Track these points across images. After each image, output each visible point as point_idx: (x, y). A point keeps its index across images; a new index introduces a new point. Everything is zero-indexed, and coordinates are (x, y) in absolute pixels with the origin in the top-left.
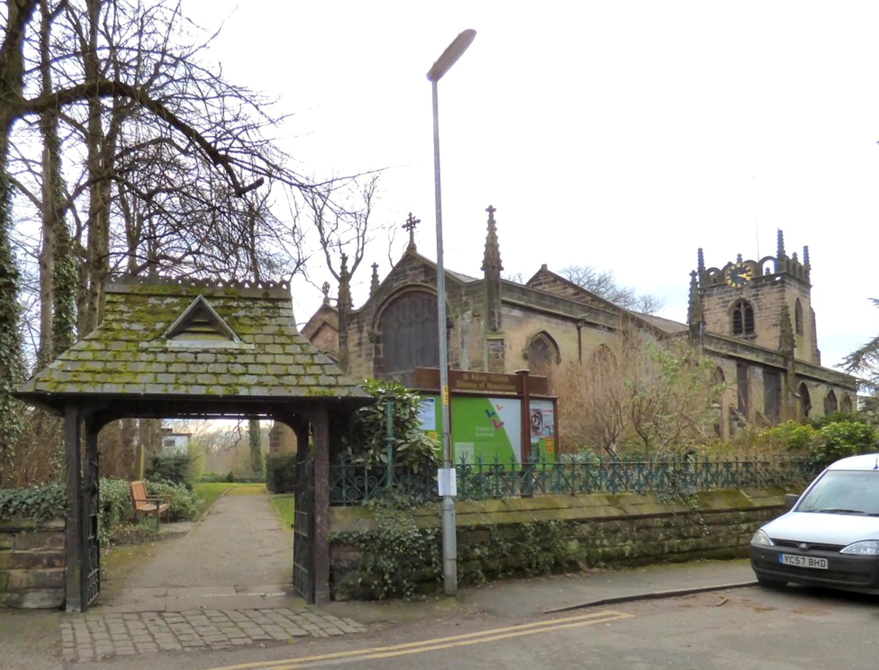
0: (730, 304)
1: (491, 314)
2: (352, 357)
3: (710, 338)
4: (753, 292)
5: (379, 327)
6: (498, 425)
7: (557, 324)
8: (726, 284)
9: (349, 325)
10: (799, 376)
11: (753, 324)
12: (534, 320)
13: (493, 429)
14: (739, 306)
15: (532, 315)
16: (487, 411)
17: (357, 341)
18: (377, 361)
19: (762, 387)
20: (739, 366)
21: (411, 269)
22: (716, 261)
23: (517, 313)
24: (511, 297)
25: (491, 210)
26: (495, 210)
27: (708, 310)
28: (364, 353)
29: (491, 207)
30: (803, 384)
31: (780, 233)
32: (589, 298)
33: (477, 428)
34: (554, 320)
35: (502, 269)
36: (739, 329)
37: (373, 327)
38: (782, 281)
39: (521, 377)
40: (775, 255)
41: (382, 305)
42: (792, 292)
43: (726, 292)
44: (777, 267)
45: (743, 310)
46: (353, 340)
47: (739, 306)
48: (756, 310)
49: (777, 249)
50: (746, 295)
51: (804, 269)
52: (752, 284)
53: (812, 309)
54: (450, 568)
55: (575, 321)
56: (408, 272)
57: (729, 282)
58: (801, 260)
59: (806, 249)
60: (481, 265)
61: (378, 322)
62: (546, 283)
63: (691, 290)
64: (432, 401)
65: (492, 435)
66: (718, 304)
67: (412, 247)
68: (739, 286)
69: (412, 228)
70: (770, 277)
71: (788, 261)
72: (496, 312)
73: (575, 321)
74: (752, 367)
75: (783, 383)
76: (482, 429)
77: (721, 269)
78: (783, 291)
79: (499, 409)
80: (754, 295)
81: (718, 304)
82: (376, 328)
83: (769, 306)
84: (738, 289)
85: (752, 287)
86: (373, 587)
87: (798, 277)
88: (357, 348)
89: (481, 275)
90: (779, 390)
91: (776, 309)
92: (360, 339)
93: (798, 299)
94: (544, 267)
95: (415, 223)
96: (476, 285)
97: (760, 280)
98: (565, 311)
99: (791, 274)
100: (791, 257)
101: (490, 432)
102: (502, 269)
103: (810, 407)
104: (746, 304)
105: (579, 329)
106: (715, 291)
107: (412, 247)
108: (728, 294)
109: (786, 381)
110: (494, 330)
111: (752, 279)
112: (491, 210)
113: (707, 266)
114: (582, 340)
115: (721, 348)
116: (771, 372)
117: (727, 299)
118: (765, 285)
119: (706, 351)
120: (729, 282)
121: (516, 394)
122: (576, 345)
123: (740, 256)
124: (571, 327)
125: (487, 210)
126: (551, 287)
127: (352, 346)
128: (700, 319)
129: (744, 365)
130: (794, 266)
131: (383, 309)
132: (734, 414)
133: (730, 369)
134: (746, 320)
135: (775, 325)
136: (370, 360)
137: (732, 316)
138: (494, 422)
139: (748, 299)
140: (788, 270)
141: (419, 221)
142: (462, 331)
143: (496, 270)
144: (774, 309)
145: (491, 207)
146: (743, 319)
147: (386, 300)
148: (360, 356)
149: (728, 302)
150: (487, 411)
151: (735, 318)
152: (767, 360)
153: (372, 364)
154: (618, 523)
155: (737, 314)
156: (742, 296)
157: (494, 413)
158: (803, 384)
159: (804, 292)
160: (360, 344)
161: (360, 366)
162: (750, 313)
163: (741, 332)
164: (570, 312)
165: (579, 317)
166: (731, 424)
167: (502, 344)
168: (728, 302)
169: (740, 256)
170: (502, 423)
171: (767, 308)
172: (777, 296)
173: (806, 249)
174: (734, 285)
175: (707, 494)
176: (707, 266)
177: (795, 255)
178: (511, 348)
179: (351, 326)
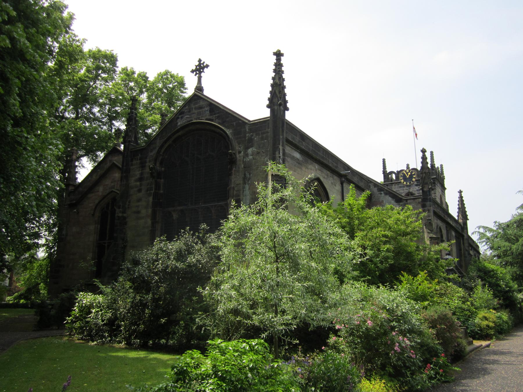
5: (161, 163)
7: (327, 175)
8: (400, 182)
9: (132, 160)
12: (310, 167)
15: (309, 161)
17: (138, 176)
21: (195, 108)
23: (297, 155)
25: (278, 55)
26: (282, 55)
29: (423, 149)
31: (384, 161)
35: (287, 109)
37: (155, 164)
41: (165, 142)
52: (416, 183)
53: (446, 203)
56: (194, 111)
60: (267, 102)
61: (161, 158)
67: (199, 89)
68: (408, 183)
69: (200, 73)
82: (158, 164)
84: (407, 186)
85: (416, 185)
86: (165, 311)
88: (138, 183)
89: (266, 113)
92: (142, 174)
95: (203, 68)
96: (261, 124)
102: (287, 109)
105: (342, 184)
107: (199, 89)
108: (402, 188)
111: (416, 180)
113: (388, 170)
120: (402, 181)
123: (408, 165)
125: (275, 54)
127: (133, 182)
131: (167, 145)
139: (414, 192)
142: (244, 167)
143: (282, 108)
145: (423, 149)
147: (170, 137)
148: (140, 191)
153: (151, 199)
156: (411, 190)
160: (141, 179)
161: (139, 200)
169: (408, 165)
175: (380, 326)
179: (134, 162)
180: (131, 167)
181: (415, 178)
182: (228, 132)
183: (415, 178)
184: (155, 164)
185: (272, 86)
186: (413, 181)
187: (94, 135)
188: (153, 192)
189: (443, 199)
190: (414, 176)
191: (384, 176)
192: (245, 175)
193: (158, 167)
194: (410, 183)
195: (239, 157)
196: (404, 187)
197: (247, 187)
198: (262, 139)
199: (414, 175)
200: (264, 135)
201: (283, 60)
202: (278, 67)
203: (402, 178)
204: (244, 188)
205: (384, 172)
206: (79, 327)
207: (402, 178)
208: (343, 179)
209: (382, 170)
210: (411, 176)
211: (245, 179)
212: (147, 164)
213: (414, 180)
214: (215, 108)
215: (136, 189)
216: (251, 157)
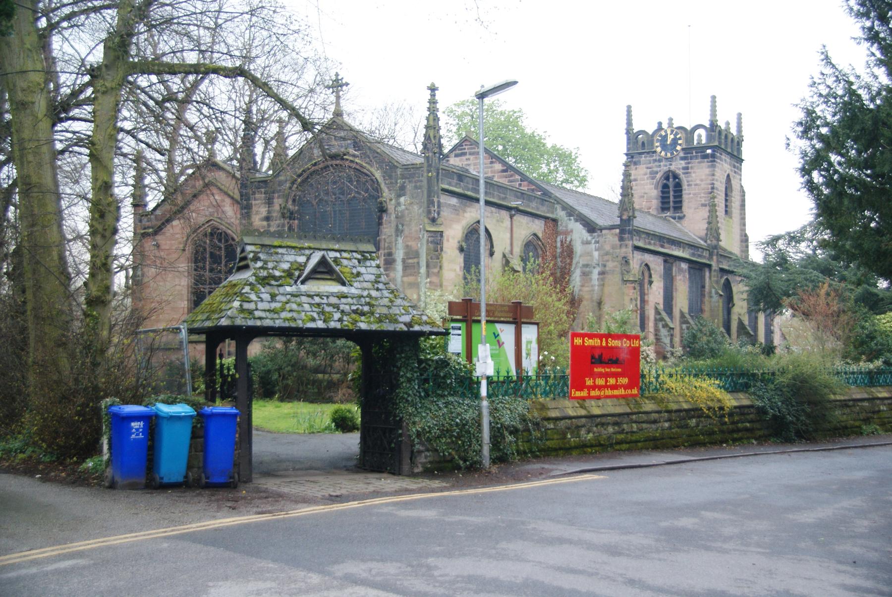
0: (658, 176)
1: (431, 203)
3: (639, 232)
8: (655, 152)
9: (254, 193)
10: (722, 270)
11: (681, 202)
12: (468, 209)
14: (667, 178)
15: (468, 203)
19: (687, 283)
20: (665, 261)
22: (645, 124)
23: (454, 201)
24: (450, 184)
25: (433, 89)
26: (437, 89)
27: (635, 180)
29: (433, 85)
30: (727, 280)
31: (714, 98)
32: (518, 177)
36: (666, 206)
38: (713, 156)
39: (517, 307)
40: (707, 124)
42: (724, 166)
44: (710, 138)
45: (671, 183)
46: (257, 213)
47: (667, 178)
48: (685, 186)
49: (709, 118)
50: (677, 166)
51: (736, 140)
52: (682, 154)
53: (742, 186)
55: (508, 209)
57: (659, 149)
58: (734, 131)
63: (623, 181)
66: (646, 174)
68: (669, 155)
70: (701, 149)
71: (720, 132)
72: (436, 199)
73: (508, 209)
74: (677, 262)
75: (707, 279)
77: (650, 133)
78: (713, 166)
80: (684, 168)
81: (646, 174)
82: (215, 123)
83: (698, 182)
85: (682, 159)
87: (729, 150)
88: (265, 223)
90: (703, 287)
91: (705, 185)
92: (269, 212)
93: (728, 176)
95: (341, 86)
97: (693, 152)
98: (500, 199)
99: (723, 147)
100: (723, 127)
103: (734, 305)
104: (676, 176)
105: (511, 217)
106: (643, 158)
108: (657, 164)
109: (710, 278)
110: (433, 220)
111: (683, 149)
112: (433, 89)
113: (636, 128)
114: (515, 229)
115: (650, 244)
116: (697, 268)
117: (655, 169)
118: (696, 157)
119: (637, 248)
120: (659, 149)
121: (511, 320)
122: (508, 235)
123: (671, 120)
124: (505, 214)
125: (429, 88)
128: (631, 214)
129: (671, 260)
130: (726, 136)
132: (660, 314)
133: (657, 265)
135: (704, 205)
137: (660, 189)
139: (677, 171)
140: (720, 143)
141: (347, 84)
142: (397, 217)
144: (703, 186)
145: (433, 85)
146: (671, 195)
149: (657, 173)
151: (663, 192)
152: (693, 255)
154: (583, 420)
155: (665, 186)
156: (673, 168)
158: (727, 280)
159: (734, 167)
162: (678, 186)
163: (668, 209)
166: (656, 325)
167: (442, 236)
168: (657, 173)
169: (671, 120)
171: (698, 178)
172: (707, 171)
174: (663, 153)
177: (728, 124)
178: (448, 240)
179: (257, 196)
180: (253, 202)
181: (680, 145)
182: (378, 175)
183: (680, 145)
184: (287, 202)
186: (677, 151)
189: (734, 182)
190: (680, 142)
191: (629, 139)
192: (397, 226)
193: (290, 205)
194: (672, 154)
195: (391, 206)
196: (660, 161)
197: (400, 240)
198: (416, 187)
199: (680, 139)
200: (418, 184)
202: (432, 105)
203: (658, 144)
204: (396, 240)
205: (629, 131)
206: (21, 415)
207: (658, 144)
208: (513, 212)
209: (625, 126)
210: (675, 141)
211: (397, 229)
212: (275, 201)
213: (679, 148)
214: (357, 139)
216: (403, 207)
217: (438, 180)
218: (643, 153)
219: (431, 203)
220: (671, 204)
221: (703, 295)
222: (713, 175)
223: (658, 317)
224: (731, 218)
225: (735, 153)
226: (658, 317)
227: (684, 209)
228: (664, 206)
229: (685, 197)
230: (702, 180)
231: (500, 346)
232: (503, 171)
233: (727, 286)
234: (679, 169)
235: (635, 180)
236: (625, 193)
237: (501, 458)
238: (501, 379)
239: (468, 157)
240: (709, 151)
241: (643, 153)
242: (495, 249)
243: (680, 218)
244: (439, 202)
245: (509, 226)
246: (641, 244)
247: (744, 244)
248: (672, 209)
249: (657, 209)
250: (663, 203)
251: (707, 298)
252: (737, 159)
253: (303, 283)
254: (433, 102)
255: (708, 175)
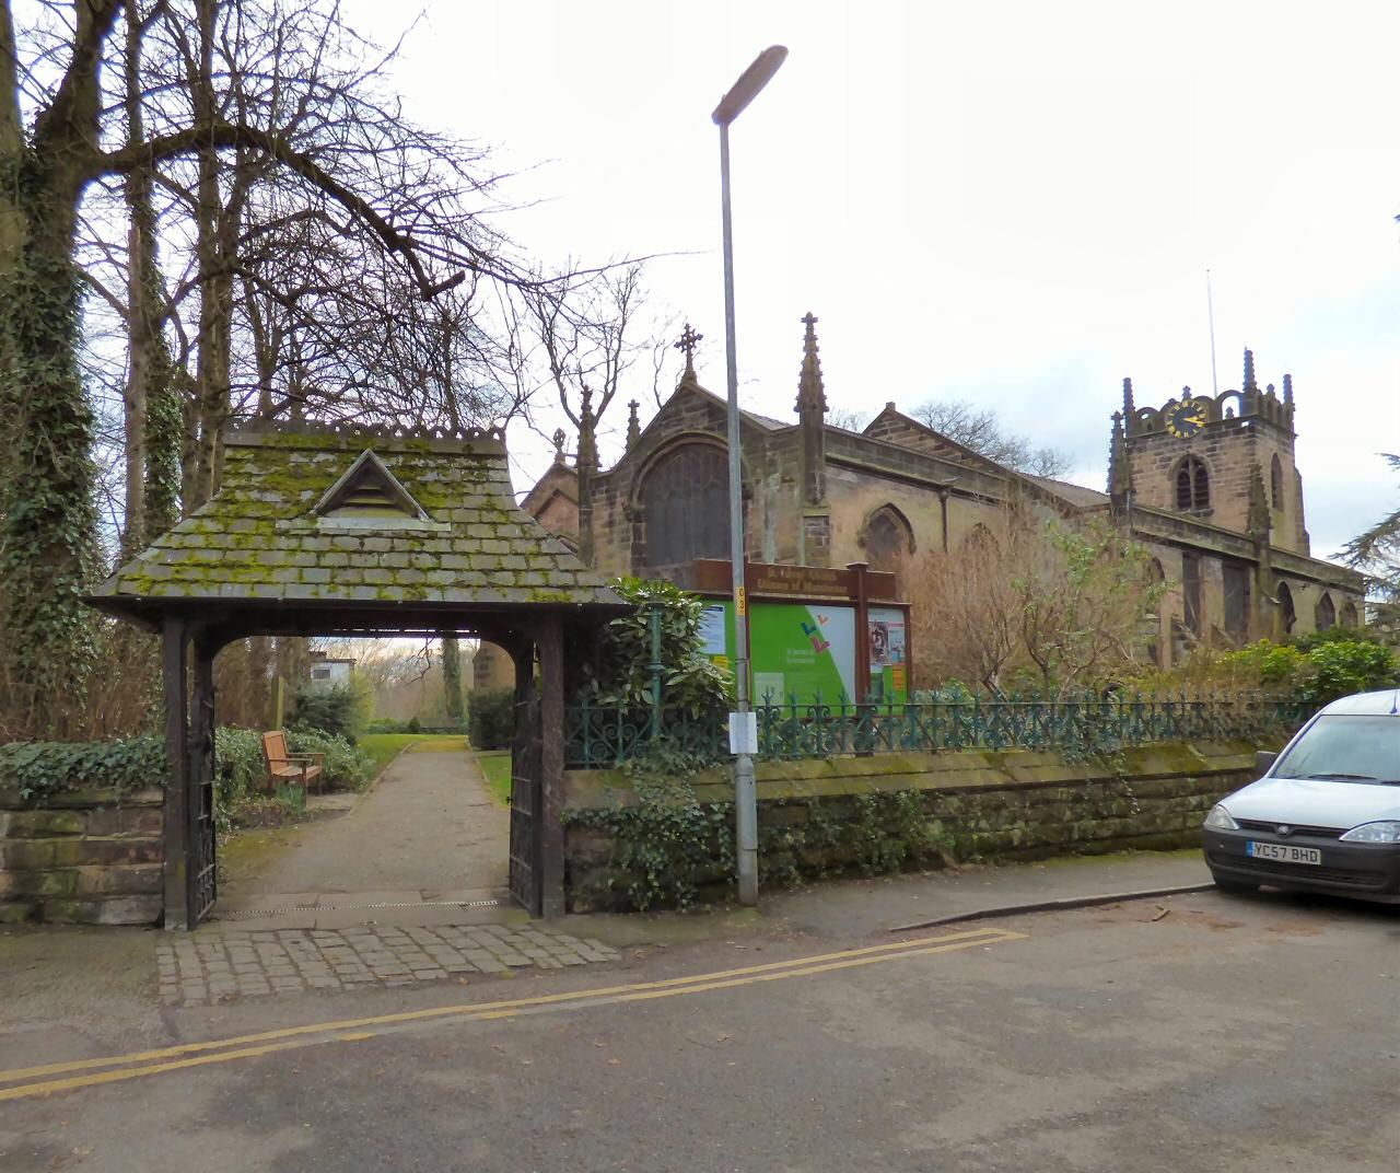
0: (1172, 463)
1: (810, 478)
2: (599, 543)
4: (1208, 444)
5: (639, 498)
6: (821, 647)
8: (1167, 433)
9: (594, 494)
10: (1276, 571)
12: (875, 487)
13: (813, 652)
15: (872, 479)
16: (803, 625)
18: (636, 549)
20: (1185, 556)
21: (687, 410)
22: (1151, 397)
23: (848, 476)
24: (840, 452)
25: (810, 320)
27: (1139, 472)
28: (617, 537)
29: (809, 315)
31: (1249, 356)
33: (789, 651)
34: (904, 487)
38: (1251, 429)
39: (856, 574)
40: (1241, 389)
41: (645, 464)
42: (1267, 445)
43: (1167, 444)
44: (1244, 407)
47: (1186, 465)
48: (1212, 472)
51: (1284, 410)
52: (1206, 432)
54: (748, 864)
55: (937, 488)
56: (684, 414)
57: (1172, 429)
58: (1280, 396)
59: (1287, 379)
60: (795, 403)
62: (893, 431)
64: (721, 609)
65: (812, 661)
68: (1186, 435)
69: (689, 348)
70: (1233, 422)
73: (937, 488)
76: (796, 652)
79: (822, 622)
80: (1208, 450)
82: (635, 499)
83: (1232, 466)
84: (1184, 440)
85: (1206, 438)
87: (1275, 422)
88: (607, 530)
89: (794, 419)
92: (611, 515)
93: (1275, 455)
94: (890, 406)
95: (694, 339)
98: (921, 472)
100: (1264, 392)
101: (808, 657)
102: (827, 410)
103: (1295, 620)
104: (1197, 462)
105: (943, 501)
106: (1150, 442)
107: (689, 376)
108: (1170, 447)
109: (1257, 580)
110: (815, 502)
111: (1206, 425)
112: (810, 320)
113: (1138, 405)
115: (1159, 530)
116: (1236, 567)
117: (1168, 455)
118: (1226, 434)
120: (1172, 429)
122: (939, 525)
123: (1187, 389)
124: (929, 494)
125: (803, 320)
126: (900, 437)
127: (598, 527)
128: (1127, 486)
129: (1194, 555)
130: (1270, 404)
131: (645, 470)
132: (1179, 629)
133: (1173, 561)
134: (1197, 488)
135: (1241, 495)
136: (625, 548)
137: (1175, 480)
138: (814, 641)
139: (1199, 455)
141: (700, 337)
143: (817, 411)
144: (1238, 470)
145: (809, 315)
146: (1192, 484)
147: (651, 457)
148: (610, 542)
149: (1170, 459)
150: (803, 625)
151: (1179, 484)
152: (1229, 547)
154: (1002, 795)
155: (1183, 479)
156: (1191, 451)
157: (814, 628)
159: (1284, 444)
160: (611, 524)
161: (610, 557)
162: (1202, 476)
163: (1188, 505)
164: (929, 475)
165: (943, 482)
166: (1173, 646)
167: (827, 523)
168: (1170, 459)
169: (1187, 389)
170: (827, 644)
171: (1228, 467)
173: (1287, 379)
174: (1178, 434)
176: (1138, 406)
177: (1271, 388)
178: (840, 530)
184: (631, 499)
185: (802, 374)
187: (124, 5)
188: (631, 543)
193: (635, 504)
201: (818, 329)
215: (605, 540)
217: (820, 447)
218: (1148, 437)
219: (810, 478)
220: (1193, 497)
221: (1246, 605)
222: (1253, 454)
223: (1177, 634)
224: (1282, 510)
225: (1284, 426)
226: (1177, 634)
227: (1211, 502)
228: (1183, 500)
229: (1213, 487)
230: (1236, 463)
231: (818, 649)
232: (938, 448)
233: (1285, 593)
234: (1202, 452)
235: (1139, 472)
236: (1118, 457)
237: (773, 883)
238: (802, 713)
239: (889, 435)
240: (1245, 424)
241: (1148, 437)
242: (917, 543)
243: (1208, 514)
244: (822, 476)
245: (940, 512)
246: (1144, 529)
247: (1302, 545)
248: (1193, 504)
249: (1172, 506)
250: (1180, 497)
251: (1253, 611)
252: (1286, 433)
253: (323, 512)
254: (810, 339)
255: (1247, 455)
